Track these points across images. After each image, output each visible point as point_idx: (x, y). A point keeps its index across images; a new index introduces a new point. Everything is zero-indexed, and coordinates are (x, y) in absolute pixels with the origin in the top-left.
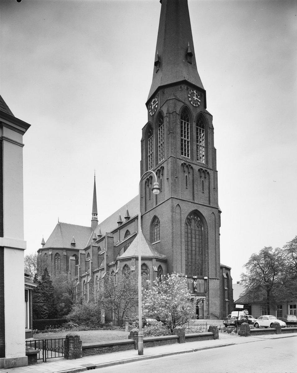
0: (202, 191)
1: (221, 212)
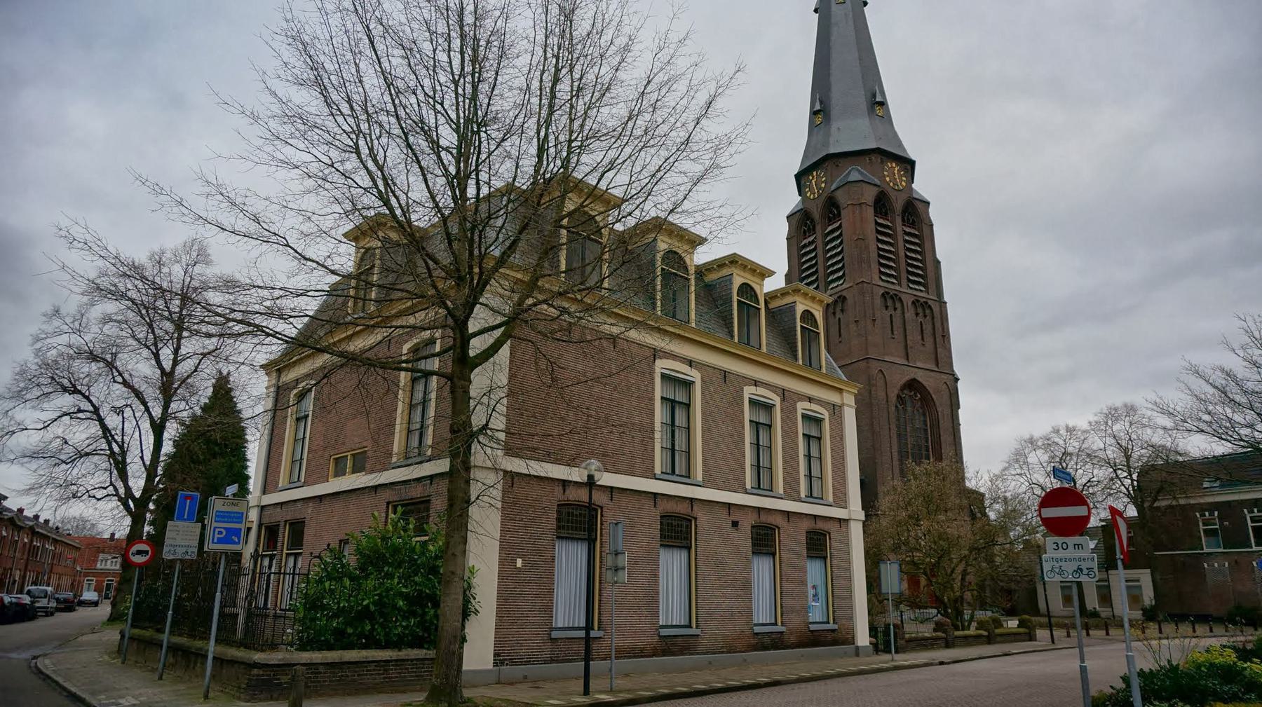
0: (921, 342)
1: (958, 379)
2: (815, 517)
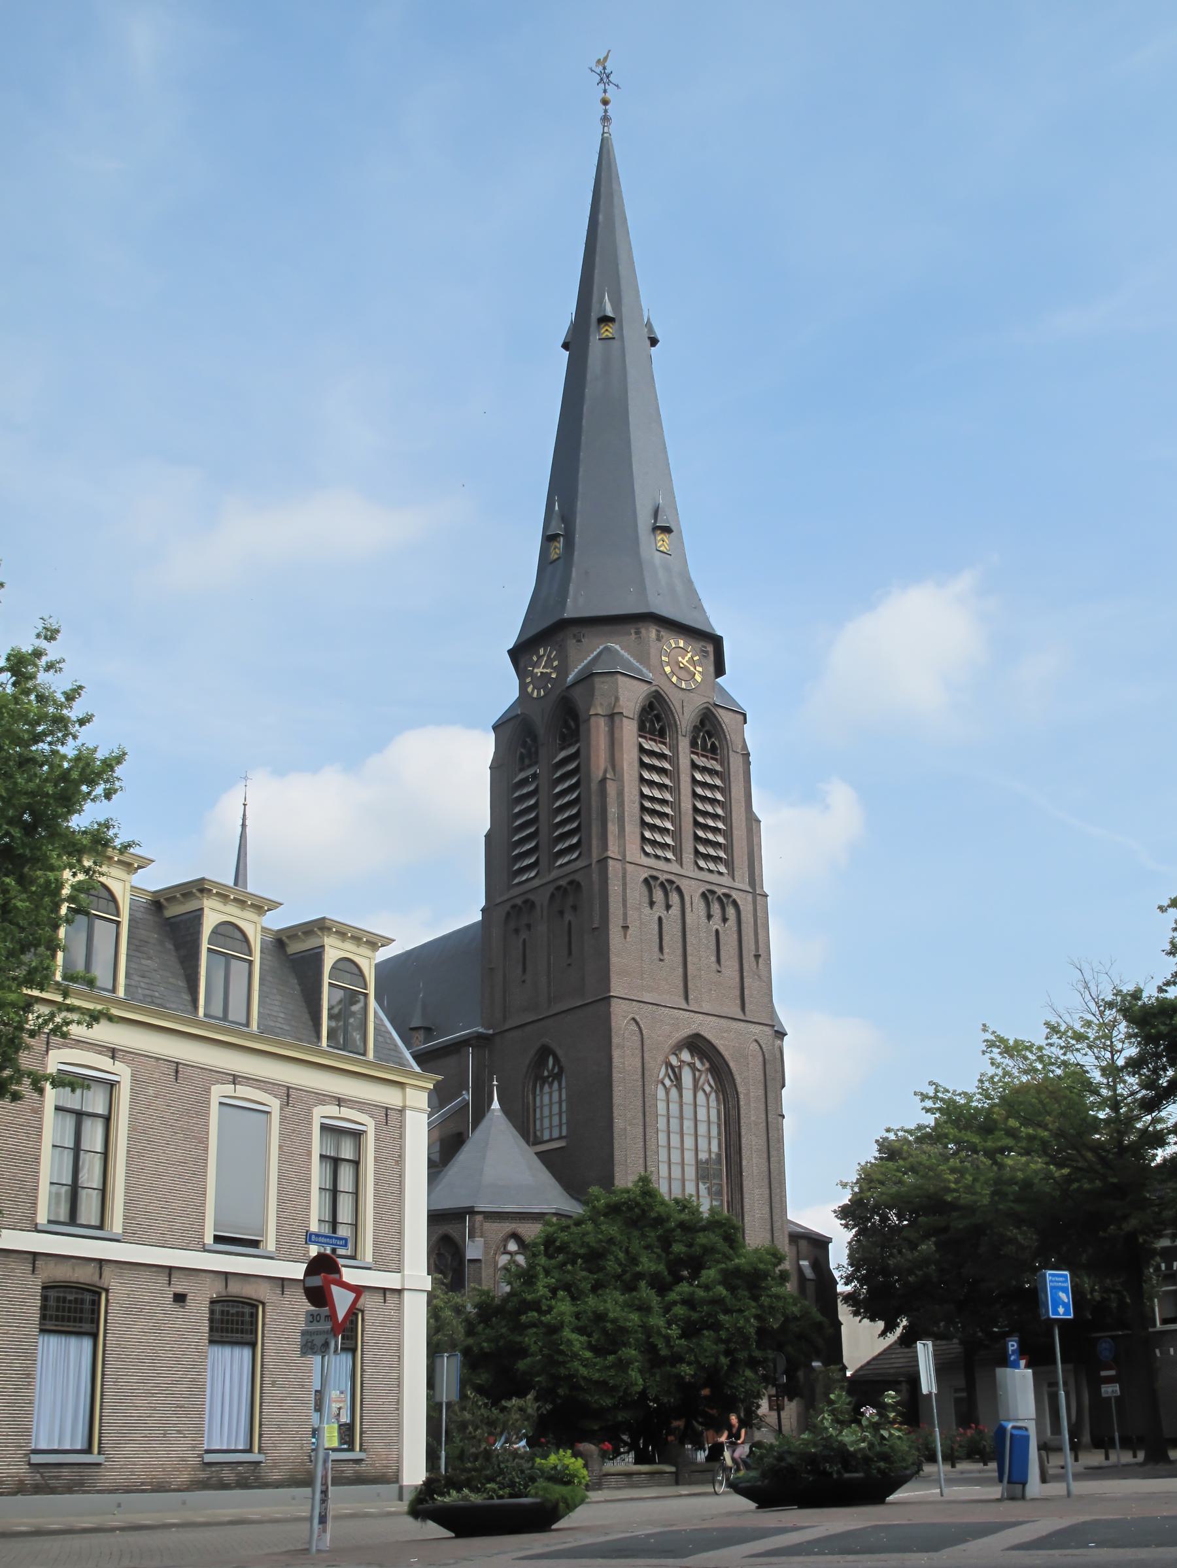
0: (715, 966)
2: (226, 1275)
